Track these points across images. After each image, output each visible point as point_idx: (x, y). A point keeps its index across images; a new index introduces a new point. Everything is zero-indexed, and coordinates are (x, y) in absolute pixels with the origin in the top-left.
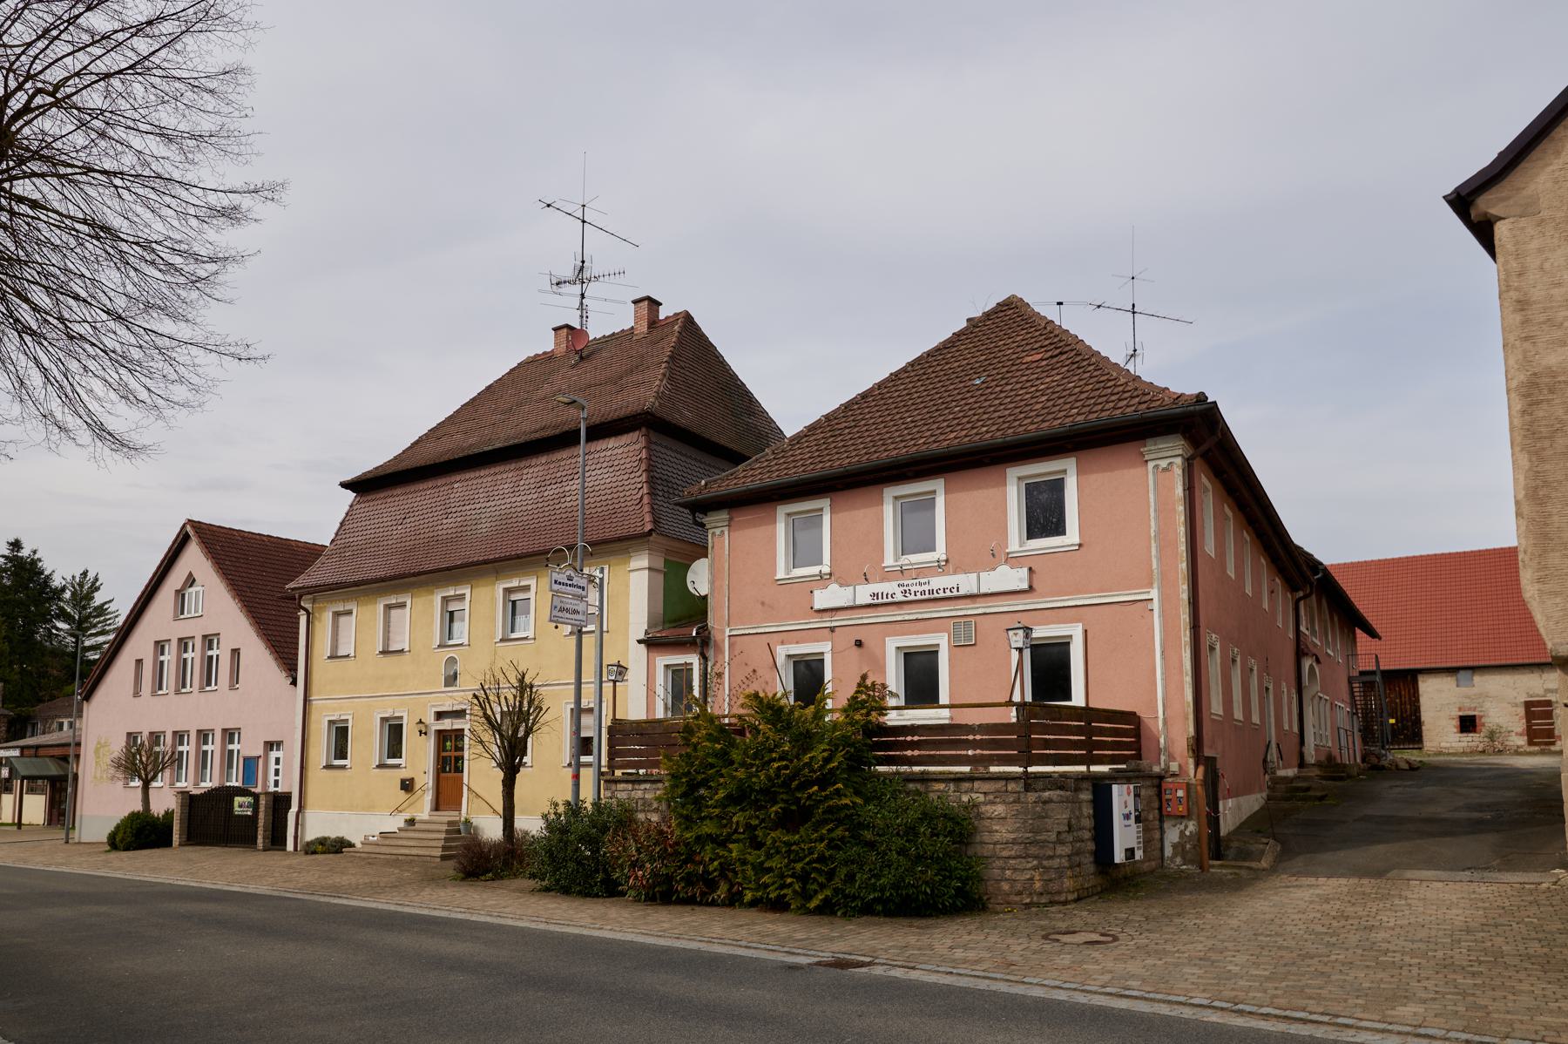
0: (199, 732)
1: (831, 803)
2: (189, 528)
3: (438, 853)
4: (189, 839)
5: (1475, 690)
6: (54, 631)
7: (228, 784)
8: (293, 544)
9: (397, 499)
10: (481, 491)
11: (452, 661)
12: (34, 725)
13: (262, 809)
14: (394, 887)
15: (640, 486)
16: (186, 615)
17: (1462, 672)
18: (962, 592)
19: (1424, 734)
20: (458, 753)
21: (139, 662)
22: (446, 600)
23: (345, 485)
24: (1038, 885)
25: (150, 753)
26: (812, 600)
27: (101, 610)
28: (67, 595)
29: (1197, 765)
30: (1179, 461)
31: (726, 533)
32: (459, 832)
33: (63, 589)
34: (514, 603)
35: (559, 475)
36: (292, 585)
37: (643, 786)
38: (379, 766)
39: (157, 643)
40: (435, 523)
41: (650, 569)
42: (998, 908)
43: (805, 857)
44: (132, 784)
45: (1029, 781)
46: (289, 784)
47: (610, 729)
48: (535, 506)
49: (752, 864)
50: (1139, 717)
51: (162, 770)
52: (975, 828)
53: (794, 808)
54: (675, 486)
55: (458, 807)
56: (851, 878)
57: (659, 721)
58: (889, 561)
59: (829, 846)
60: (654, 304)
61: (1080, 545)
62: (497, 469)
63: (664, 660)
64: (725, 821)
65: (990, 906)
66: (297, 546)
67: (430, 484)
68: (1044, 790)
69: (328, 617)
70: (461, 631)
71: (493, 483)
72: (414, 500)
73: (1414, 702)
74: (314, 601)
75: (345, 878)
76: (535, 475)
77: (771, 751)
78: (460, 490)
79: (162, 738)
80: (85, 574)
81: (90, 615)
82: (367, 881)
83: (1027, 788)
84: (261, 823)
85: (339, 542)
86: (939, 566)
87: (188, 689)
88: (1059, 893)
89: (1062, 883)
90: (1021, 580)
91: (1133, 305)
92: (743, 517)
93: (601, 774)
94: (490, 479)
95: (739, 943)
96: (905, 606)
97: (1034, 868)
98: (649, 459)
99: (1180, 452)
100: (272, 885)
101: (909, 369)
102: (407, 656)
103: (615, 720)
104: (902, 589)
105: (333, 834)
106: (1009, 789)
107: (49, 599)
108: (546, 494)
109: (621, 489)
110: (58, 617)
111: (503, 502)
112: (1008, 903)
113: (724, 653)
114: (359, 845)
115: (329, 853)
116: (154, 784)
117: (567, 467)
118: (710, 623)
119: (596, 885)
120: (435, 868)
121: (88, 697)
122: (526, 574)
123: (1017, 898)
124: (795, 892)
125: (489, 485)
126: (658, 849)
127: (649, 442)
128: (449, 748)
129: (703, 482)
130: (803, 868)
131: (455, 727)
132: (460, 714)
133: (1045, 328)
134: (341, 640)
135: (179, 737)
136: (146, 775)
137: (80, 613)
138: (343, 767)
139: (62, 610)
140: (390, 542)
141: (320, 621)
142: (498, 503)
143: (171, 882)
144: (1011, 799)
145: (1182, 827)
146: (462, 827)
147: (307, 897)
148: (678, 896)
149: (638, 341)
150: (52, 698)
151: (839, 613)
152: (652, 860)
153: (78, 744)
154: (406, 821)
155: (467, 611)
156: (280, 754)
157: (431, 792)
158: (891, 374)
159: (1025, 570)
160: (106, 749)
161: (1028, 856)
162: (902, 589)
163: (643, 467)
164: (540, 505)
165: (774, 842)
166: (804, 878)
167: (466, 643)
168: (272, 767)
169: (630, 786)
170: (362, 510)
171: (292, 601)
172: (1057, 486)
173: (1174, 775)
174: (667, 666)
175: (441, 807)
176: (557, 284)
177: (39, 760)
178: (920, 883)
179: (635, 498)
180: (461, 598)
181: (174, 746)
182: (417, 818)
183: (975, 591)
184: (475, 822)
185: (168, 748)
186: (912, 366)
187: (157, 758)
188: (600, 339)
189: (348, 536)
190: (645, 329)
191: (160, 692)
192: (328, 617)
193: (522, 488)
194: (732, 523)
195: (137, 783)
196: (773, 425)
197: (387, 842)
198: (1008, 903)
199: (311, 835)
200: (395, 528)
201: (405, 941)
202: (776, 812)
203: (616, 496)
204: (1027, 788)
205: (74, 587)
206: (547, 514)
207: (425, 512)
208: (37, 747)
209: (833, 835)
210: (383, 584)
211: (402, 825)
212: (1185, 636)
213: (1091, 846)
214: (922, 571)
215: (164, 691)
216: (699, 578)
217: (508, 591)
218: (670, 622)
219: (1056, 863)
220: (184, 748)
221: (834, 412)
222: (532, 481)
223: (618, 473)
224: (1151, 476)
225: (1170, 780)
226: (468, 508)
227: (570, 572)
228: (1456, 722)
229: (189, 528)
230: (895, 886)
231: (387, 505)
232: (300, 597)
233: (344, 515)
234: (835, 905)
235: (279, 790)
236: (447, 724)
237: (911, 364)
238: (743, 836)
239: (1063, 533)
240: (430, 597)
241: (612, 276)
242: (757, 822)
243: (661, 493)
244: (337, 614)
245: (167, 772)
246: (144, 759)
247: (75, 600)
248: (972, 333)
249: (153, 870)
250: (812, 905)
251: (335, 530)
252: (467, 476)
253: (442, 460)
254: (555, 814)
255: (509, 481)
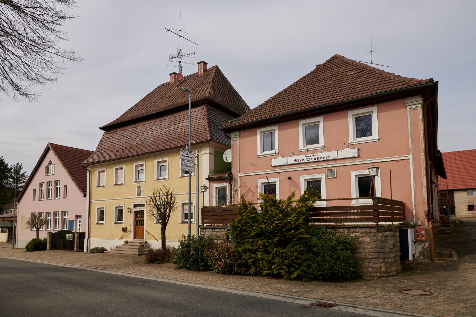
0: (54, 212)
1: (300, 236)
2: (49, 146)
3: (137, 253)
4: (52, 248)
5: (474, 196)
6: (9, 182)
7: (64, 229)
8: (83, 151)
9: (119, 132)
10: (148, 128)
11: (139, 187)
12: (3, 211)
13: (76, 238)
14: (125, 266)
15: (205, 124)
16: (49, 174)
17: (469, 190)
18: (331, 158)
19: (456, 211)
20: (142, 219)
21: (35, 190)
22: (137, 166)
23: (101, 128)
24: (383, 269)
25: (39, 219)
26: (271, 163)
27: (23, 175)
28: (12, 170)
29: (428, 221)
30: (420, 106)
31: (238, 140)
32: (143, 246)
33: (11, 169)
34: (160, 166)
35: (175, 122)
36: (84, 162)
37: (216, 230)
38: (115, 223)
39: (40, 183)
40: (132, 140)
41: (210, 153)
42: (367, 278)
43: (289, 258)
44: (33, 229)
45: (378, 228)
46: (84, 229)
47: (202, 209)
48: (167, 133)
49: (266, 260)
50: (404, 204)
51: (43, 225)
52: (357, 247)
53: (283, 239)
54: (217, 125)
55: (142, 237)
56: (309, 266)
57: (214, 207)
58: (301, 147)
59: (299, 254)
60: (205, 64)
61: (379, 139)
62: (153, 121)
63: (215, 185)
64: (254, 244)
65: (364, 277)
66: (84, 152)
67: (130, 127)
68: (384, 232)
69: (96, 173)
70: (142, 176)
71: (152, 126)
72: (125, 133)
73: (453, 200)
74: (92, 168)
75: (106, 262)
76: (167, 122)
77: (274, 217)
78: (141, 128)
79: (42, 214)
80: (18, 164)
81: (19, 177)
82: (114, 263)
83: (378, 231)
84: (75, 242)
85: (99, 148)
86: (323, 149)
87: (50, 198)
88: (391, 272)
89: (392, 268)
90: (355, 153)
91: (372, 61)
92: (244, 134)
93: (199, 226)
94: (151, 124)
95: (270, 293)
96: (308, 164)
97: (382, 263)
98: (208, 115)
99: (421, 102)
100: (82, 265)
101: (301, 80)
102: (123, 186)
103: (204, 206)
104: (307, 158)
105: (100, 246)
106: (371, 231)
107: (7, 172)
108: (171, 129)
109: (198, 126)
110: (10, 177)
111: (156, 132)
112: (372, 276)
113: (238, 183)
114: (109, 250)
115: (99, 253)
116: (40, 229)
117: (178, 119)
118: (233, 172)
119: (201, 267)
120: (137, 259)
121: (19, 201)
122: (165, 157)
123: (375, 274)
124: (285, 271)
125: (151, 126)
126: (227, 254)
127: (208, 109)
128: (138, 217)
129: (229, 122)
130: (288, 262)
131: (141, 210)
132: (143, 205)
133: (353, 63)
134: (101, 181)
135: (48, 214)
136: (38, 227)
137: (16, 176)
138: (103, 224)
139: (11, 175)
140: (117, 147)
141: (94, 174)
142: (154, 132)
143: (47, 263)
144: (372, 235)
145: (423, 245)
146: (144, 244)
147: (94, 270)
148: (234, 272)
149: (200, 76)
150: (9, 203)
151: (281, 167)
152: (225, 258)
153: (16, 217)
154: (125, 242)
155: (144, 170)
156: (80, 219)
157: (133, 232)
158: (295, 83)
159: (356, 149)
160: (25, 218)
161: (379, 258)
162: (307, 158)
163: (206, 118)
164: (169, 132)
165: (276, 252)
166: (289, 266)
167: (144, 181)
168: (78, 224)
169: (211, 230)
170: (107, 137)
171: (85, 168)
172: (369, 117)
173: (419, 225)
174: (216, 188)
175: (136, 237)
176: (172, 58)
177: (4, 222)
178: (339, 268)
179: (204, 128)
180: (142, 165)
181: (46, 217)
182: (128, 241)
183: (336, 158)
184: (148, 242)
185: (44, 218)
186: (302, 79)
187: (41, 221)
188: (186, 77)
189: (102, 145)
190: (202, 73)
191: (41, 200)
192: (96, 173)
193: (162, 127)
194: (240, 136)
195: (35, 229)
196: (246, 105)
197: (119, 249)
198: (372, 276)
199: (92, 247)
200: (118, 142)
201: (138, 291)
202: (277, 241)
203: (196, 128)
204: (378, 231)
205: (14, 168)
206: (172, 135)
207: (129, 136)
208: (4, 218)
209: (300, 249)
210: (115, 161)
211: (123, 243)
212: (424, 172)
213: (400, 254)
214: (314, 151)
215: (43, 199)
216: (228, 156)
217: (158, 163)
218: (217, 172)
219: (389, 260)
220: (49, 218)
221: (275, 96)
222: (166, 124)
223: (197, 120)
224: (408, 112)
225: (418, 227)
226: (144, 134)
227: (187, 152)
228: (467, 207)
229: (49, 146)
230: (330, 269)
231: (116, 135)
232: (87, 166)
233: (101, 139)
234: (302, 276)
235: (80, 231)
236: (138, 209)
237: (302, 79)
238: (262, 250)
239: (371, 135)
240: (131, 165)
241: (190, 55)
242: (268, 244)
243: (212, 127)
244: (100, 172)
245: (44, 226)
246: (37, 221)
247: (15, 172)
248: (323, 67)
249: (41, 259)
250: (293, 276)
251: (98, 144)
252: (143, 123)
253: (134, 118)
254: (184, 240)
255: (158, 125)
